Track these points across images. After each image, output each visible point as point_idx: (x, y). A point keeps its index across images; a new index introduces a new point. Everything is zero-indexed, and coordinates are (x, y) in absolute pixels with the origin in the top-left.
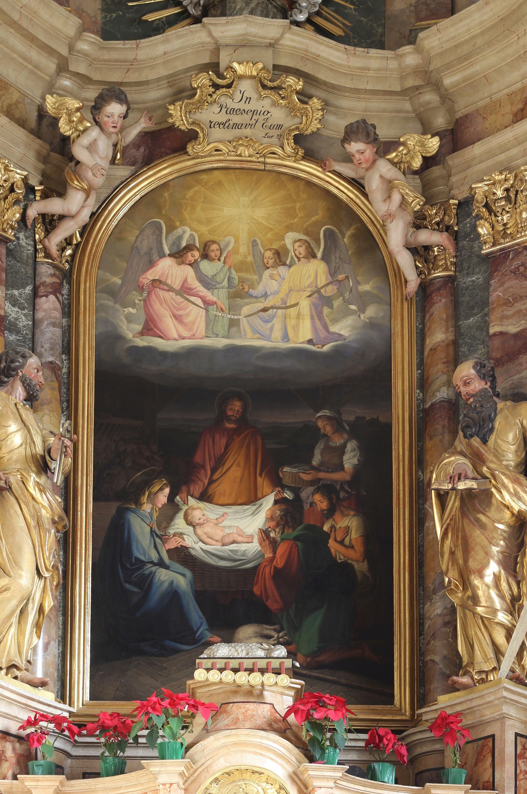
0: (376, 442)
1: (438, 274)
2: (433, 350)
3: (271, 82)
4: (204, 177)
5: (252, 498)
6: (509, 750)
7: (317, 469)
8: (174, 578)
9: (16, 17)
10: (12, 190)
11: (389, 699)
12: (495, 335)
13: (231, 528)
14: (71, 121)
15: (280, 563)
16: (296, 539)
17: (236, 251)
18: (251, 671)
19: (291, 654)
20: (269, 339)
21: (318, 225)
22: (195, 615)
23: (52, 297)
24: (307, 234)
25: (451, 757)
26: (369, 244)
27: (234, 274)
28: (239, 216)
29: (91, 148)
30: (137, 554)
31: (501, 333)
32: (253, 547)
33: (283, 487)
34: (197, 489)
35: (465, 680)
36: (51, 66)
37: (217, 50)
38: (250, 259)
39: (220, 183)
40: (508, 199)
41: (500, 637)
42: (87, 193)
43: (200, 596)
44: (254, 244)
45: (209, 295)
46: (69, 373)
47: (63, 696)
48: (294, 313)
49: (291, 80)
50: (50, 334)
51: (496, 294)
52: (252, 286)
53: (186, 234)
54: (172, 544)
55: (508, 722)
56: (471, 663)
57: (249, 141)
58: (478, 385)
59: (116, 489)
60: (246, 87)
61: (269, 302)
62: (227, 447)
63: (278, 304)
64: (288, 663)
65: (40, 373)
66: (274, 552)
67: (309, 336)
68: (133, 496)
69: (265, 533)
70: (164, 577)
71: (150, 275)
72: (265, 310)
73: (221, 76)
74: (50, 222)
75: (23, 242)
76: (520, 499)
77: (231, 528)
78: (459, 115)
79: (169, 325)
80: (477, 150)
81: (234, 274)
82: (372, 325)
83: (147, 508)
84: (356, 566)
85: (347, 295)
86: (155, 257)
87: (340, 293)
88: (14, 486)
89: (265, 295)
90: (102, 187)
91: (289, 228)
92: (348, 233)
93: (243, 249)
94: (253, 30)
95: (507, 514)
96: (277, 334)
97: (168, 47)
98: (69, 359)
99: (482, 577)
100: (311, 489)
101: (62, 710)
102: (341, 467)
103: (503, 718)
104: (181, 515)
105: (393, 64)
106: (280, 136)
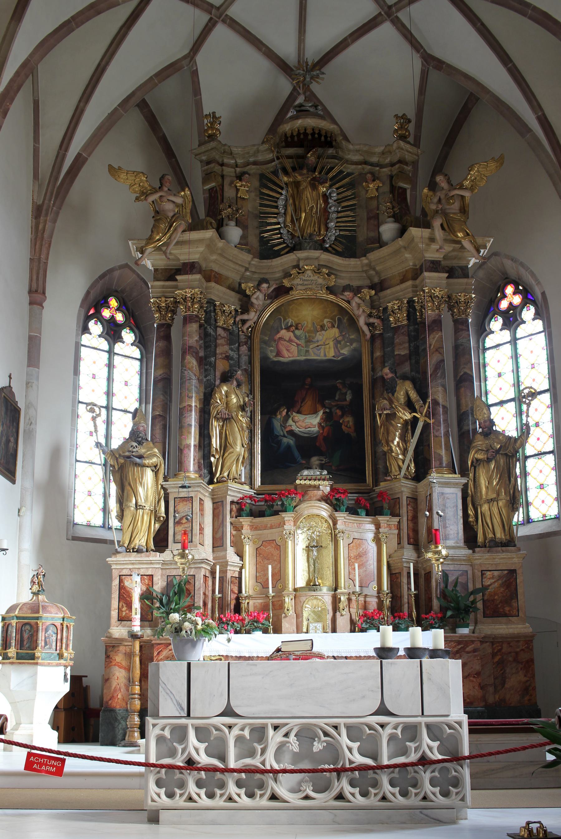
0: (358, 391)
1: (377, 332)
2: (376, 358)
3: (317, 271)
4: (296, 301)
5: (315, 412)
6: (405, 503)
7: (337, 401)
8: (289, 441)
9: (231, 258)
10: (231, 313)
11: (365, 481)
12: (397, 355)
13: (308, 423)
14: (250, 290)
15: (325, 434)
16: (331, 425)
17: (307, 326)
18: (315, 480)
19: (329, 473)
20: (319, 356)
21: (335, 316)
22: (296, 453)
23: (245, 346)
24: (331, 319)
25: (386, 505)
26: (353, 322)
27: (307, 335)
28: (308, 314)
29: (257, 299)
30: (276, 433)
31: (399, 355)
32: (316, 429)
33: (326, 408)
34: (296, 409)
35: (389, 478)
36: (243, 270)
37: (299, 260)
38: (312, 329)
39: (301, 303)
40: (399, 309)
41: (401, 464)
42: (256, 312)
43: (298, 447)
44: (313, 323)
45: (298, 342)
46: (251, 371)
47: (251, 484)
48: (327, 347)
49: (324, 270)
50: (244, 359)
51: (397, 341)
52: (313, 338)
53: (290, 321)
54: (288, 429)
55: (404, 493)
56: (391, 472)
57: (311, 289)
58: (390, 375)
59: (268, 412)
60: (309, 272)
61: (319, 344)
62: (306, 394)
63: (322, 344)
64: (328, 477)
65: (234, 327)
66: (323, 430)
67: (333, 355)
68: (274, 413)
69: (320, 424)
70: (285, 440)
71: (278, 336)
72: (318, 346)
73: (300, 270)
74: (244, 322)
75: (234, 329)
76: (405, 415)
77: (308, 423)
78: (382, 278)
79: (285, 353)
80: (388, 291)
81: (307, 335)
82: (355, 350)
83: (279, 417)
84: (352, 434)
85: (346, 340)
86: (280, 330)
87: (344, 339)
88: (234, 417)
89: (318, 341)
90: (262, 311)
91: (325, 318)
92: (346, 318)
93: (310, 325)
94: (311, 254)
95: (402, 420)
96: (322, 354)
97: (282, 261)
98: (251, 366)
99: (393, 443)
100: (336, 408)
101: (252, 492)
102: (345, 400)
103: (402, 492)
104: (291, 419)
105: (359, 263)
106: (321, 287)
